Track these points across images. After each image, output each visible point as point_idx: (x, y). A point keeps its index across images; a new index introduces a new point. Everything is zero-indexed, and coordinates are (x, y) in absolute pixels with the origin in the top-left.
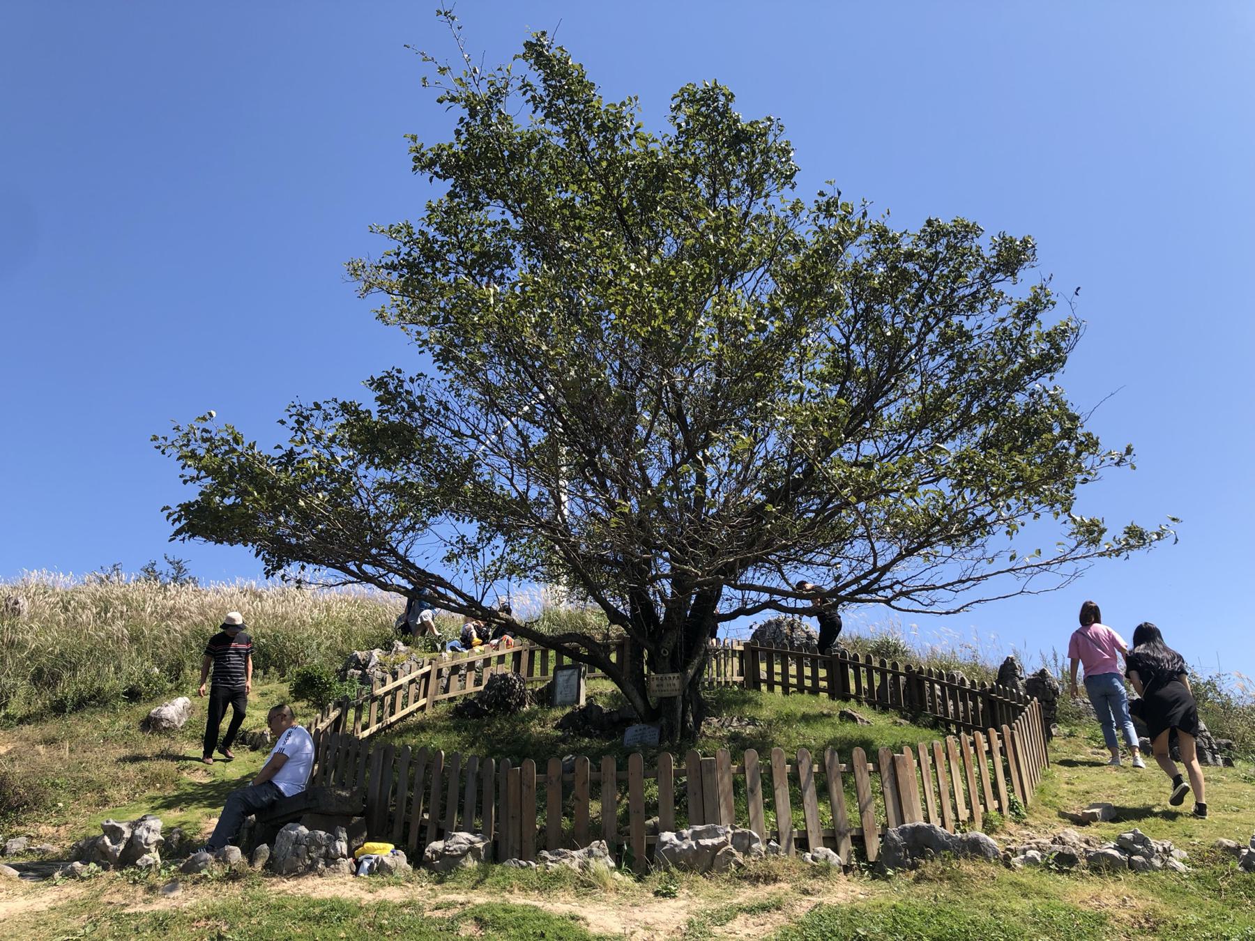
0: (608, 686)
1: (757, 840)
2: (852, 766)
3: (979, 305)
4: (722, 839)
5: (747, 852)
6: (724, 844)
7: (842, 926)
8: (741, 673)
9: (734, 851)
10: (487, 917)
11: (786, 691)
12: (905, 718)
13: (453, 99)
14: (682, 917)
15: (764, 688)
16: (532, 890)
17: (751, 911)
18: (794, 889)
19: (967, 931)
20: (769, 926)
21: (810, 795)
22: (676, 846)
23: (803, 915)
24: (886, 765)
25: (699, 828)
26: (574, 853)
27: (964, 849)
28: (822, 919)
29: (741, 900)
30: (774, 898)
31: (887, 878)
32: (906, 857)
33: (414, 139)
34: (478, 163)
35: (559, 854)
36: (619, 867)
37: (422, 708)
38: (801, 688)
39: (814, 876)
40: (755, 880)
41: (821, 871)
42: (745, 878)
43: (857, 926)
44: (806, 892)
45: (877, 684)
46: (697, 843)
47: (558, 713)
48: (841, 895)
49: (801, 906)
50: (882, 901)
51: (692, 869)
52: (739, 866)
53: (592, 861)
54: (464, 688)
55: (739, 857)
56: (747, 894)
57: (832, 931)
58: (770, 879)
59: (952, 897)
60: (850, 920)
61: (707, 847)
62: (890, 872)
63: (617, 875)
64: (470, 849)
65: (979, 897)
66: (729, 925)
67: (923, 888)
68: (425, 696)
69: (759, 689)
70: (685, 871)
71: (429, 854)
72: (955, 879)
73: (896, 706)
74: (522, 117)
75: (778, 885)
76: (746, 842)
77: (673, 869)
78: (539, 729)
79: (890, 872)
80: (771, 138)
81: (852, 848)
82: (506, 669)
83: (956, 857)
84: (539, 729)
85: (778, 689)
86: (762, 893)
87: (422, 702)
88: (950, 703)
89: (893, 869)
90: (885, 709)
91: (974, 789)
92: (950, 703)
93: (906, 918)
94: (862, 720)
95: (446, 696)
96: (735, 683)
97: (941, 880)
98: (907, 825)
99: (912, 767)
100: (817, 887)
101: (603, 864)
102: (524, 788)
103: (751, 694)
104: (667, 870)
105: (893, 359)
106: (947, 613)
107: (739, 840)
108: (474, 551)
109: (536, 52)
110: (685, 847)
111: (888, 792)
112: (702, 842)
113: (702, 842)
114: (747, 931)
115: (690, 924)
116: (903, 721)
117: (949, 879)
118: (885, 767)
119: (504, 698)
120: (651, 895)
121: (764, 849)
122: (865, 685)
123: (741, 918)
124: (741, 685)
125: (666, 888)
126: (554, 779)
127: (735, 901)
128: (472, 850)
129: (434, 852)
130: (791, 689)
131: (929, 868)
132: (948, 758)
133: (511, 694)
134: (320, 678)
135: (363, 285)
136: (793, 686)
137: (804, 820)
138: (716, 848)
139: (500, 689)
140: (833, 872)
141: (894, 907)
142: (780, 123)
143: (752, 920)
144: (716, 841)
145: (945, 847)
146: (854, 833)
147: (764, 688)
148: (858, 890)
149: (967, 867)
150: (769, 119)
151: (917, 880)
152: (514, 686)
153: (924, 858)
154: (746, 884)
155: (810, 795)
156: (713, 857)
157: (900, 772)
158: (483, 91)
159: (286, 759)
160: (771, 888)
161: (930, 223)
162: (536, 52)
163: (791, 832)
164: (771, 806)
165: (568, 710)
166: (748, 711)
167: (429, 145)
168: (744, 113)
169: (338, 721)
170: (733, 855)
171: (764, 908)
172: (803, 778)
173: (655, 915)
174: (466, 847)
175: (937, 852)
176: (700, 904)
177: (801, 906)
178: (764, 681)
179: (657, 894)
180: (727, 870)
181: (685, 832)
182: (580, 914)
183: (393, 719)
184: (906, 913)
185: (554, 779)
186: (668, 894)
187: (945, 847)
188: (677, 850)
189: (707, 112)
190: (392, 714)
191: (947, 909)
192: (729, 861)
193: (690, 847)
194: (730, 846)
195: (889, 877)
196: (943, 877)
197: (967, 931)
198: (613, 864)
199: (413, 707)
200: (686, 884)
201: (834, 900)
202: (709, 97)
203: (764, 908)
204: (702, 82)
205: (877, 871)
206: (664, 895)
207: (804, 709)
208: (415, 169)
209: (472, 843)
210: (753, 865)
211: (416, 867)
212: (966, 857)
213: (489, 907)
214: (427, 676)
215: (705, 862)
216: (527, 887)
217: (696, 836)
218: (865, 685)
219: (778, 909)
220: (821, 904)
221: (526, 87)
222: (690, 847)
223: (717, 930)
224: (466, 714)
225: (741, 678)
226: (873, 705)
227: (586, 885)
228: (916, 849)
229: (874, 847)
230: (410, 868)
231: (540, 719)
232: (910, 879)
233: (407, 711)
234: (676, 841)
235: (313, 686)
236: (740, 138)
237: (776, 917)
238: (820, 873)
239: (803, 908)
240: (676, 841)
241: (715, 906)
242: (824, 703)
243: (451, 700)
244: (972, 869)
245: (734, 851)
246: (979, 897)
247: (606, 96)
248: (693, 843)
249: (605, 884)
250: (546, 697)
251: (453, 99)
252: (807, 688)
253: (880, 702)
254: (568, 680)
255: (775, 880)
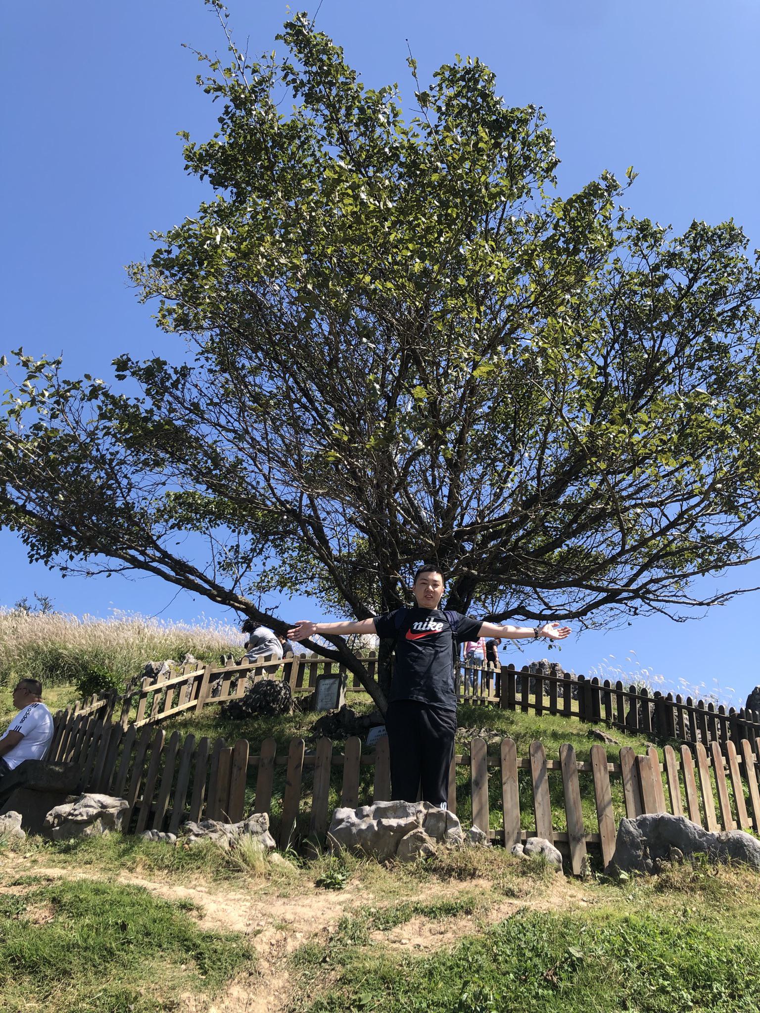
0: (367, 699)
1: (455, 824)
2: (591, 765)
3: (737, 323)
4: (411, 819)
5: (441, 837)
6: (414, 826)
7: (551, 942)
8: (497, 695)
9: (425, 835)
10: (68, 897)
11: (539, 713)
12: (653, 741)
13: (219, 89)
14: (334, 915)
15: (518, 708)
16: (160, 869)
17: (431, 913)
18: (495, 888)
19: (729, 962)
20: (449, 935)
21: (542, 797)
22: (353, 825)
23: (496, 923)
24: (630, 774)
25: (383, 804)
26: (227, 826)
27: (722, 851)
28: (523, 930)
29: (422, 897)
30: (465, 899)
31: (620, 883)
32: (645, 856)
33: (186, 136)
34: (245, 158)
35: (208, 827)
36: (280, 846)
37: (193, 708)
38: (553, 710)
39: (524, 873)
40: (446, 873)
41: (533, 868)
42: (435, 871)
43: (569, 944)
44: (510, 893)
45: (627, 709)
46: (379, 823)
47: (314, 717)
48: (556, 900)
49: (498, 910)
50: (610, 910)
51: (369, 855)
52: (430, 854)
53: (246, 837)
54: (336, 751)
55: (431, 844)
56: (433, 891)
57: (534, 949)
58: (465, 873)
59: (707, 912)
60: (563, 935)
61: (390, 828)
62: (624, 875)
63: (276, 857)
64: (99, 815)
65: (744, 916)
66: (396, 930)
67: (668, 898)
68: (196, 697)
69: (514, 709)
70: (361, 857)
71: (50, 818)
72: (711, 891)
73: (644, 730)
74: (286, 106)
75: (474, 882)
76: (442, 825)
77: (346, 855)
78: (294, 730)
79: (624, 875)
80: (531, 126)
81: (587, 856)
82: (277, 677)
83: (712, 862)
84: (294, 730)
85: (532, 711)
86: (452, 891)
87: (193, 703)
88: (698, 731)
89: (628, 871)
90: (633, 733)
91: (726, 801)
92: (698, 731)
93: (642, 937)
94: (610, 741)
95: (217, 699)
96: (490, 702)
97: (692, 889)
98: (648, 815)
99: (657, 770)
100: (525, 887)
101: (255, 840)
102: (235, 770)
103: (507, 713)
104: (337, 855)
105: (649, 376)
106: (701, 604)
107: (432, 821)
108: (247, 561)
109: (297, 35)
110: (364, 827)
111: (630, 796)
112: (385, 822)
113: (385, 822)
114: (418, 940)
115: (342, 925)
116: (651, 744)
117: (703, 888)
118: (627, 770)
119: (268, 703)
120: (312, 885)
121: (463, 835)
122: (615, 712)
123: (416, 921)
124: (498, 704)
125: (332, 877)
126: (266, 761)
127: (414, 899)
128: (103, 815)
129: (58, 816)
130: (544, 712)
131: (676, 872)
132: (697, 765)
133: (275, 700)
134: (104, 677)
135: (143, 291)
136: (546, 709)
137: (536, 823)
138: (402, 830)
139: (265, 694)
140: (549, 869)
141: (626, 920)
142: (542, 111)
143: (429, 926)
144: (403, 822)
145: (698, 847)
146: (589, 839)
147: (518, 708)
148: (580, 895)
149: (726, 875)
150: (531, 107)
151: (660, 888)
152: (279, 692)
153: (669, 859)
154: (434, 878)
155: (542, 797)
156: (398, 843)
157: (644, 774)
158: (248, 80)
159: (22, 737)
160: (465, 885)
161: (694, 226)
162: (297, 35)
163: (519, 833)
164: (496, 804)
165: (324, 714)
166: (500, 725)
167: (200, 141)
168: (507, 98)
169: (102, 711)
170: (423, 840)
171: (450, 910)
172: (536, 774)
173: (299, 909)
174: (93, 811)
175: (687, 853)
176: (368, 899)
177: (498, 910)
178: (519, 703)
179: (319, 883)
180: (413, 859)
181: (367, 809)
182: (195, 902)
183: (162, 716)
184: (644, 930)
185: (266, 761)
186: (329, 884)
187: (698, 847)
188: (354, 830)
189: (469, 94)
190: (161, 710)
191: (700, 929)
192: (418, 848)
193: (371, 827)
194: (421, 829)
195: (623, 881)
196: (692, 886)
197: (729, 962)
198: (271, 843)
199: (182, 707)
200: (357, 874)
201: (545, 906)
202: (471, 76)
203: (450, 910)
204: (467, 62)
205: (608, 875)
206: (327, 886)
207: (555, 728)
208: (187, 168)
209: (103, 806)
210: (444, 853)
211: (31, 834)
212: (725, 862)
213: (68, 887)
214: (199, 679)
215: (386, 848)
216: (155, 865)
217: (380, 814)
218: (615, 712)
219: (468, 912)
220: (525, 910)
221: (287, 70)
222: (371, 827)
223: (378, 936)
224: (231, 713)
225: (498, 699)
226: (621, 729)
227: (230, 868)
228: (661, 846)
229: (609, 852)
230: (23, 833)
231: (297, 722)
232: (651, 886)
233: (176, 710)
234: (354, 819)
235: (98, 684)
236: (501, 125)
237: (462, 923)
238: (532, 870)
239: (500, 913)
240: (354, 819)
241: (386, 903)
242: (575, 724)
243: (221, 703)
244: (734, 877)
245: (425, 835)
246: (744, 916)
247: (368, 83)
248: (375, 823)
249: (253, 867)
250: (308, 705)
251: (219, 89)
252: (559, 711)
253: (628, 727)
254: (329, 689)
255: (473, 875)
